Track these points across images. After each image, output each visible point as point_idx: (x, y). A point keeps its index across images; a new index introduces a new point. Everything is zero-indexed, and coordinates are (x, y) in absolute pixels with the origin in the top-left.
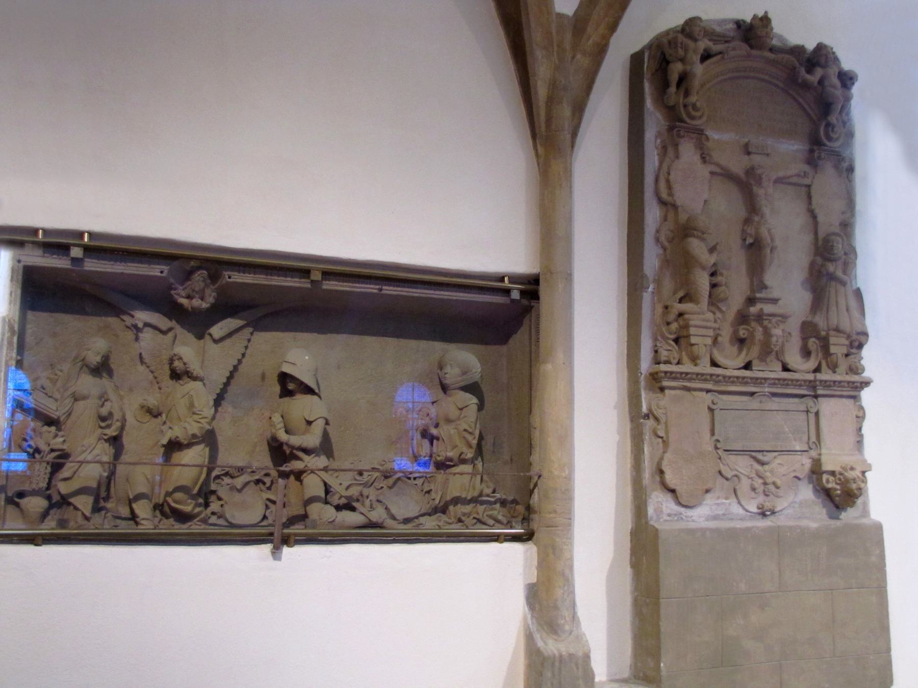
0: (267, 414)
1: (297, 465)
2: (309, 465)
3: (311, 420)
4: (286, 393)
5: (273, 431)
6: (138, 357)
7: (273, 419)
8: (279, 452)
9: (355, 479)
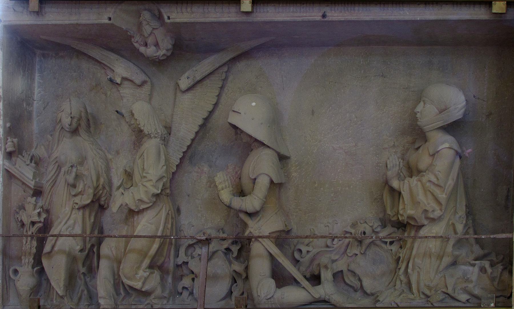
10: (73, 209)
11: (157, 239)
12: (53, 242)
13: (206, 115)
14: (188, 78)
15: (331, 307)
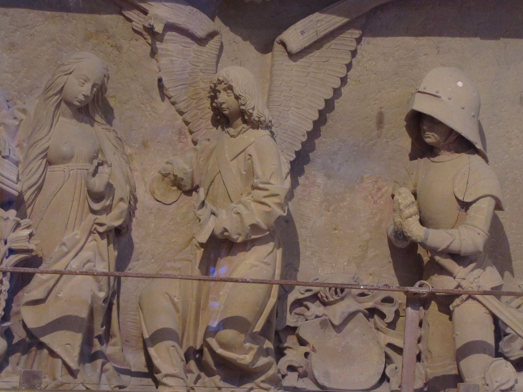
0: (388, 189)
1: (441, 284)
2: (464, 284)
3: (468, 200)
4: (422, 150)
5: (398, 220)
10: (91, 233)
11: (274, 286)
12: (51, 283)
13: (330, 94)
14: (302, 33)
15: (180, 338)
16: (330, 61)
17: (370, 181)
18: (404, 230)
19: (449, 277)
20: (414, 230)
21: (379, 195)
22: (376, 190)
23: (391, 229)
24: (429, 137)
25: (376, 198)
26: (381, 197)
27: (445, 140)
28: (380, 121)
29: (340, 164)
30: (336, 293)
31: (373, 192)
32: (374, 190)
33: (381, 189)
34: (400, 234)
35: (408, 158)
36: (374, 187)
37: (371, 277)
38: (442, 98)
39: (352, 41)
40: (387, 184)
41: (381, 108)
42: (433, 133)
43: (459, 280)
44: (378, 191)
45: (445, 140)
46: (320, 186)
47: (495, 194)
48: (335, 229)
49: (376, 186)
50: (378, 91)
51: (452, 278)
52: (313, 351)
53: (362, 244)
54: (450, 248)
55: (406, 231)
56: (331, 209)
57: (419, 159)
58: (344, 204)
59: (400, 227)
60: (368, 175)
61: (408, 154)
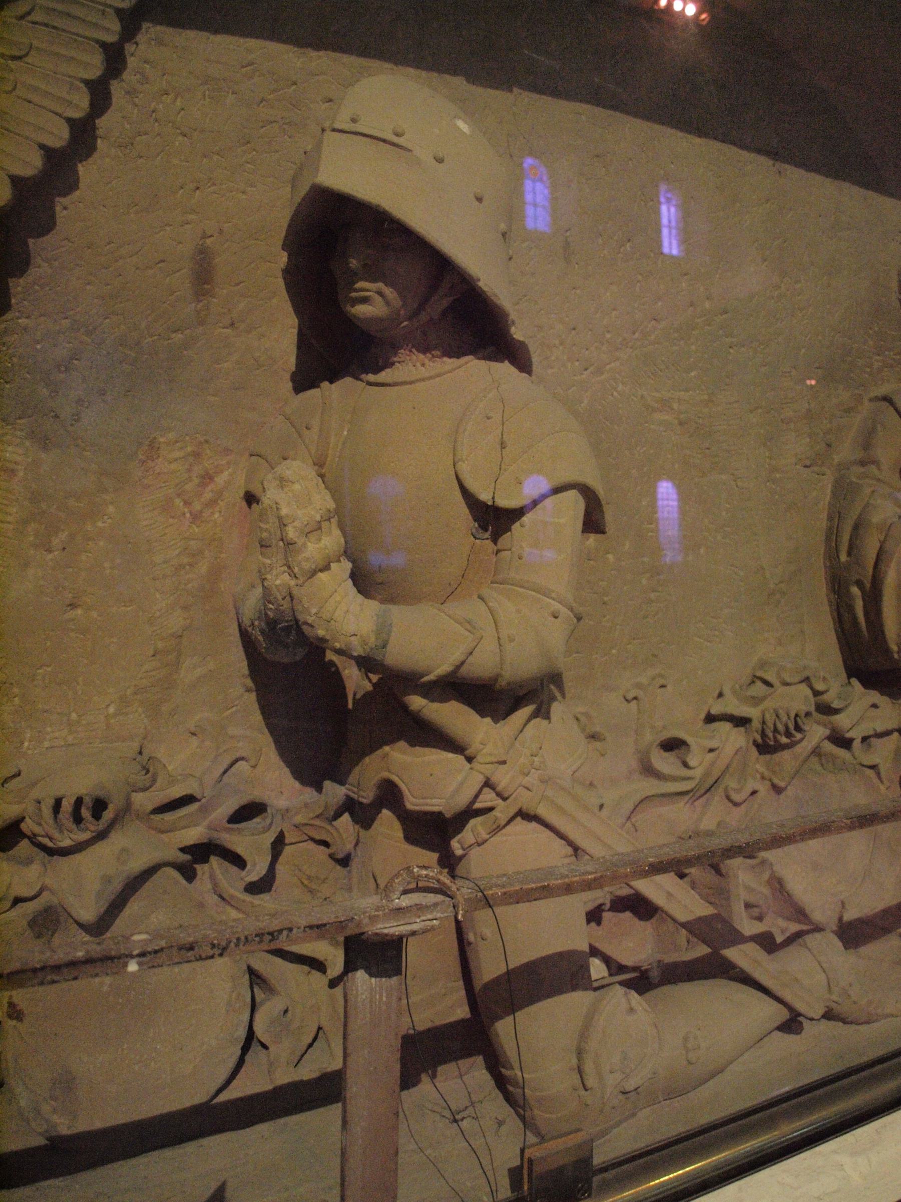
0: (232, 479)
1: (430, 779)
2: (503, 778)
3: (505, 502)
4: (335, 350)
5: (279, 580)
6: (51, 802)
7: (271, 495)
8: (327, 709)
9: (649, 770)
16: (29, 59)
17: (178, 454)
18: (301, 617)
19: (451, 755)
20: (339, 614)
21: (208, 495)
22: (196, 481)
23: (252, 602)
24: (365, 300)
25: (197, 506)
26: (213, 503)
27: (416, 313)
28: (203, 276)
29: (79, 401)
30: (78, 819)
31: (188, 487)
32: (190, 479)
33: (211, 479)
34: (287, 629)
35: (290, 385)
36: (189, 471)
37: (194, 741)
38: (415, 152)
39: (103, 12)
40: (229, 463)
41: (205, 236)
42: (380, 285)
43: (488, 770)
44: (203, 485)
45: (416, 313)
46: (13, 472)
47: (581, 479)
48: (73, 606)
49: (198, 470)
50: (193, 186)
51: (460, 758)
52: (10, 1017)
53: (160, 645)
54: (464, 670)
55: (310, 620)
56: (55, 542)
57: (325, 385)
58: (100, 524)
59: (286, 605)
60: (171, 436)
61: (287, 376)
